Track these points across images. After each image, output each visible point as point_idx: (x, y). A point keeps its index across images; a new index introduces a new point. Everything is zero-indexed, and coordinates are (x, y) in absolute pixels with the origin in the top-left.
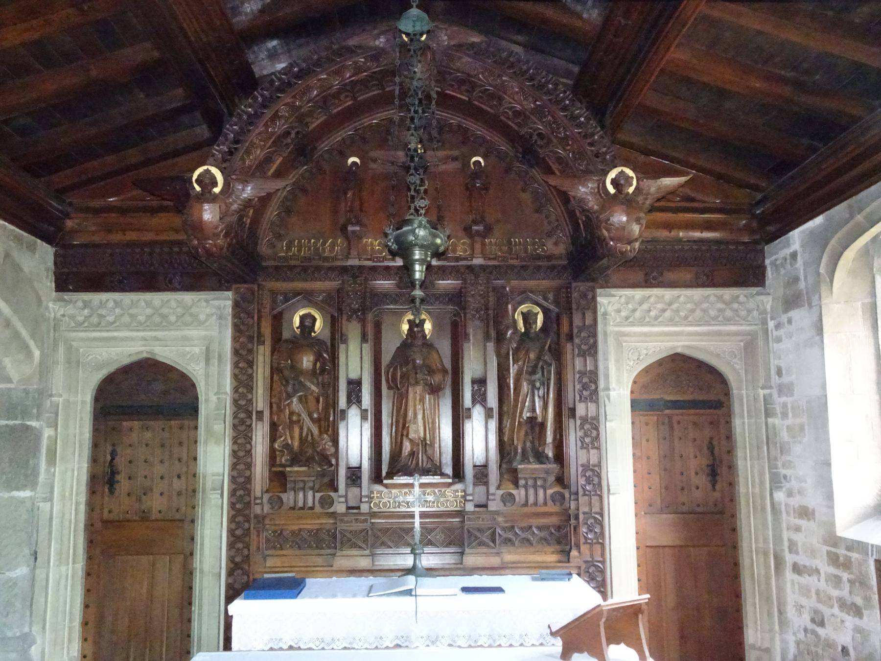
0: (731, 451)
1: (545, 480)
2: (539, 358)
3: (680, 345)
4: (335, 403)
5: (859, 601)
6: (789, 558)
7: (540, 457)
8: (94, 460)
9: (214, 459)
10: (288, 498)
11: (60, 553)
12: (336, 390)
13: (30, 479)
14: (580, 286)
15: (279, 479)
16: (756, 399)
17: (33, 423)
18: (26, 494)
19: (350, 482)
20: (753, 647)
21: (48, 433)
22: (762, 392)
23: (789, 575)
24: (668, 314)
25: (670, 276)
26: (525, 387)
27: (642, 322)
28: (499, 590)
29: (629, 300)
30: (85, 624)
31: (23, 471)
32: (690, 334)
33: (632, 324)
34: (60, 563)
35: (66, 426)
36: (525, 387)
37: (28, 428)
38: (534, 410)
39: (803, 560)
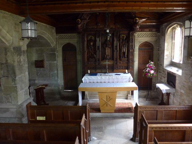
0: (153, 56)
1: (125, 60)
2: (125, 43)
3: (146, 40)
4: (96, 50)
5: (165, 76)
6: (159, 71)
7: (125, 57)
8: (63, 57)
9: (79, 57)
10: (90, 63)
11: (60, 69)
12: (96, 48)
13: (55, 60)
14: (131, 33)
15: (88, 60)
16: (157, 49)
17: (55, 53)
18: (55, 62)
19: (123, 63)
20: (153, 82)
21: (57, 54)
22: (158, 47)
23: (159, 73)
24: (70, 37)
25: (145, 30)
26: (123, 47)
27: (61, 39)
28: (119, 75)
29: (60, 36)
30: (64, 78)
31: (153, 65)
32: (148, 39)
33: (139, 37)
34: (60, 71)
35: (59, 53)
36: (123, 47)
37: (55, 53)
38: (124, 50)
39: (160, 71)
